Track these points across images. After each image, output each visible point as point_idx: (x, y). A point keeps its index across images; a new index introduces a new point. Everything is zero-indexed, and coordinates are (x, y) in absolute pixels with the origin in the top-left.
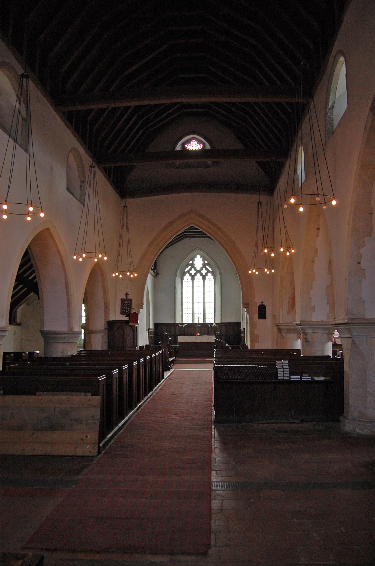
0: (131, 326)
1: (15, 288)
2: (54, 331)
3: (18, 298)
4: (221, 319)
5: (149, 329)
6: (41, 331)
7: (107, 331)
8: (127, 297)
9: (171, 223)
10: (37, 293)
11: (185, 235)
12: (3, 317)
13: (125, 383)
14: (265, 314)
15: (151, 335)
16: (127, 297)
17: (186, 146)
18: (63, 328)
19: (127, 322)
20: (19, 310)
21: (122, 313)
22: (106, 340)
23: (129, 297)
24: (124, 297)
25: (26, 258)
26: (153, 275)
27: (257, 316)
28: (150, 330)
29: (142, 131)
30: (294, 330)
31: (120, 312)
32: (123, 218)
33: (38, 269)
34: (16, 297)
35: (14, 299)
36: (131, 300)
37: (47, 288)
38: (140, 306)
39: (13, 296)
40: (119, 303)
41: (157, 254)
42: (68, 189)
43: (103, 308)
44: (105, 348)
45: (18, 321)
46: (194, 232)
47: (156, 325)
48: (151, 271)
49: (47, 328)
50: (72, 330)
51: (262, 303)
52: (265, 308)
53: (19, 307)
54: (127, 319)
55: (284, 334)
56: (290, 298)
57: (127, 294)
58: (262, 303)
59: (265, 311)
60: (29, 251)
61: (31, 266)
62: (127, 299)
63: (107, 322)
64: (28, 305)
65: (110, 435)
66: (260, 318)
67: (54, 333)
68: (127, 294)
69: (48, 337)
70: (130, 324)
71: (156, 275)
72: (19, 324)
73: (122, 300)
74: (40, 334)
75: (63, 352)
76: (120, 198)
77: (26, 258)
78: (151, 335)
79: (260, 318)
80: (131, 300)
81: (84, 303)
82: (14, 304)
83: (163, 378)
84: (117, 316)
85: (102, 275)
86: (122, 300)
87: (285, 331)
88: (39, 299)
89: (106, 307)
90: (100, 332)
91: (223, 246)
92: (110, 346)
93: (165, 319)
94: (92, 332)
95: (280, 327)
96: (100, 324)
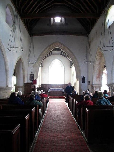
2: (2, 87)
7: (24, 87)
9: (49, 46)
11: (52, 53)
13: (33, 116)
17: (63, 18)
19: (32, 84)
21: (30, 80)
23: (33, 74)
24: (31, 74)
27: (81, 82)
29: (39, 10)
30: (98, 87)
31: (34, 76)
32: (31, 41)
36: (33, 75)
38: (37, 77)
40: (29, 76)
41: (42, 60)
42: (6, 21)
43: (23, 78)
48: (40, 66)
50: (8, 87)
51: (84, 77)
52: (85, 79)
54: (32, 82)
55: (94, 89)
56: (97, 75)
57: (32, 73)
58: (84, 77)
62: (32, 75)
63: (24, 83)
65: (26, 117)
66: (83, 82)
68: (32, 73)
70: (33, 84)
71: (42, 67)
73: (30, 75)
76: (30, 36)
79: (83, 82)
80: (33, 75)
81: (14, 74)
84: (28, 81)
85: (22, 64)
86: (30, 75)
87: (95, 88)
89: (24, 77)
90: (22, 87)
91: (27, 80)
92: (25, 93)
94: (19, 87)
95: (93, 86)
96: (21, 84)
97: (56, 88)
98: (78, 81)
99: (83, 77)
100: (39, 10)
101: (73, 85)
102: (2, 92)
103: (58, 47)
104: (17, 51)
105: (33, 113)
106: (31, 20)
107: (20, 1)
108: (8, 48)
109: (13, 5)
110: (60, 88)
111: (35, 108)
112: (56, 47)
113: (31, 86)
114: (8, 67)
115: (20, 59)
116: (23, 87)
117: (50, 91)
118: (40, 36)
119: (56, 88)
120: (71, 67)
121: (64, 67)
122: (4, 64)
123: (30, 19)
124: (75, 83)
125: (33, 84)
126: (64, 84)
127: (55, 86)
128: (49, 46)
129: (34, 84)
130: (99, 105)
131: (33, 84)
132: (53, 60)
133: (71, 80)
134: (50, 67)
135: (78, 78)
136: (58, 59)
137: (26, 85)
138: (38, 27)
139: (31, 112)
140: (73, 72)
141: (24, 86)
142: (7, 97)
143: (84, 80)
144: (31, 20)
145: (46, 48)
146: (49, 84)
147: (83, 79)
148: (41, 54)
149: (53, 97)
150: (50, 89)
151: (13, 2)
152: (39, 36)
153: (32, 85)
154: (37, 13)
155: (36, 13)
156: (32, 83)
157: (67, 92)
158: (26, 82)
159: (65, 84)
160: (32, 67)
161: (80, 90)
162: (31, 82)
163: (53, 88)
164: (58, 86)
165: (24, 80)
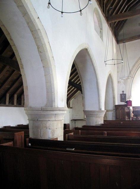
0: (128, 107)
1: (68, 87)
3: (70, 96)
6: (84, 111)
7: (115, 110)
10: (81, 91)
12: (62, 100)
16: (123, 93)
18: (97, 109)
20: (71, 101)
22: (114, 115)
23: (124, 93)
24: (122, 93)
25: (74, 69)
33: (81, 76)
34: (69, 95)
35: (69, 96)
36: (125, 94)
37: (87, 87)
39: (68, 95)
40: (119, 96)
44: (114, 119)
45: (71, 106)
49: (87, 109)
53: (71, 100)
54: (126, 103)
60: (74, 62)
61: (77, 74)
62: (123, 94)
64: (75, 99)
67: (91, 112)
68: (123, 92)
69: (89, 114)
70: (128, 106)
72: (71, 108)
74: (83, 112)
75: (96, 122)
77: (74, 69)
80: (125, 94)
82: (68, 99)
84: (118, 102)
88: (82, 93)
90: (111, 111)
92: (116, 118)
96: (111, 107)
100: (127, 6)
102: (93, 118)
104: (114, 64)
106: (117, 22)
107: (105, 2)
108: (105, 62)
109: (99, 7)
113: (124, 109)
114: (100, 85)
115: (110, 75)
116: (113, 111)
118: (130, 42)
122: (96, 81)
123: (116, 22)
129: (129, 106)
131: (128, 106)
137: (117, 107)
138: (125, 30)
141: (114, 109)
142: (100, 123)
144: (117, 22)
151: (99, 4)
153: (126, 108)
154: (124, 12)
155: (118, 13)
156: (126, 105)
158: (117, 104)
160: (123, 85)
162: (123, 103)
165: (114, 102)
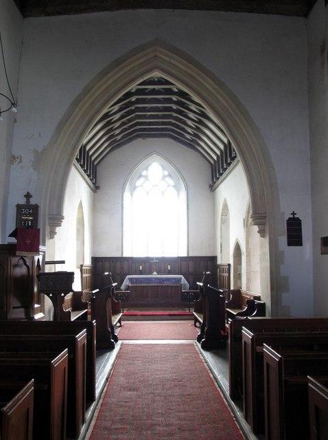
4: (188, 251)
5: (82, 266)
8: (28, 201)
14: (300, 237)
15: (84, 275)
16: (28, 201)
17: (115, 320)
23: (33, 201)
24: (23, 201)
26: (92, 189)
27: (283, 239)
28: (84, 268)
36: (36, 208)
46: (150, 124)
47: (95, 260)
51: (294, 214)
57: (28, 196)
58: (294, 214)
59: (300, 230)
66: (289, 244)
68: (28, 196)
73: (19, 207)
78: (84, 275)
80: (36, 208)
83: (90, 397)
86: (19, 207)
93: (108, 252)
97: (155, 273)
98: (266, 241)
99: (288, 216)
101: (226, 258)
103: (163, 70)
105: (80, 346)
110: (170, 272)
111: (87, 331)
112: (150, 70)
117: (128, 288)
119: (155, 275)
120: (212, 187)
121: (187, 189)
124: (238, 248)
125: (14, 255)
126: (185, 255)
127: (147, 264)
128: (117, 63)
130: (114, 285)
132: (137, 164)
133: (213, 237)
134: (127, 195)
135: (264, 224)
136: (159, 154)
139: (44, 374)
140: (225, 206)
143: (294, 233)
145: (103, 74)
146: (124, 256)
147: (288, 223)
148: (76, 103)
149: (139, 313)
150: (131, 280)
152: (66, 16)
157: (198, 291)
159: (190, 256)
160: (31, 170)
161: (277, 283)
163: (141, 273)
164: (162, 264)
